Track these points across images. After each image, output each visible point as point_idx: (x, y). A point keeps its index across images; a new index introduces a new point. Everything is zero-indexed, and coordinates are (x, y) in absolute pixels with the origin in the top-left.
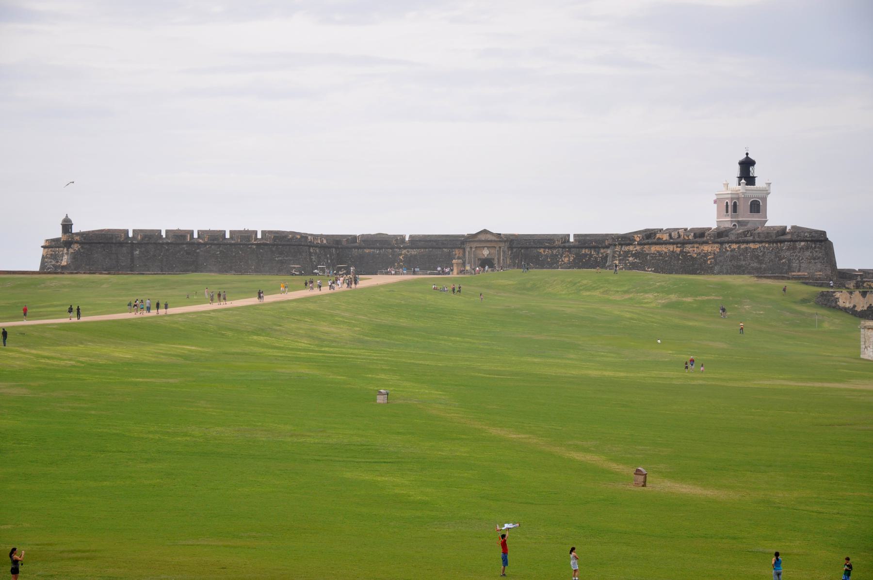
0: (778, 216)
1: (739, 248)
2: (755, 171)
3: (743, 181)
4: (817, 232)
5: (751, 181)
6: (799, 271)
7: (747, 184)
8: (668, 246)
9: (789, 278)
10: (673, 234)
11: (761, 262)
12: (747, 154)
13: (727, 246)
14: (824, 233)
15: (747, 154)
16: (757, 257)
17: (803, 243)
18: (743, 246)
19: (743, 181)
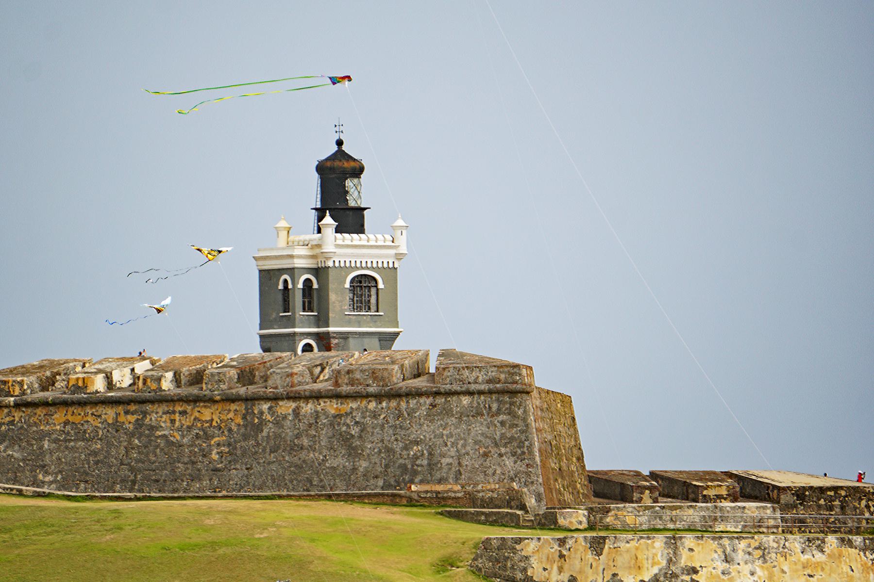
0: (428, 327)
1: (296, 412)
2: (359, 192)
3: (328, 220)
4: (501, 366)
5: (351, 220)
6: (331, 489)
7: (337, 231)
8: (100, 409)
9: (411, 502)
10: (116, 376)
11: (353, 452)
12: (340, 143)
13: (265, 406)
14: (566, 401)
15: (340, 143)
16: (346, 439)
17: (466, 400)
18: (308, 408)
19: (328, 220)
